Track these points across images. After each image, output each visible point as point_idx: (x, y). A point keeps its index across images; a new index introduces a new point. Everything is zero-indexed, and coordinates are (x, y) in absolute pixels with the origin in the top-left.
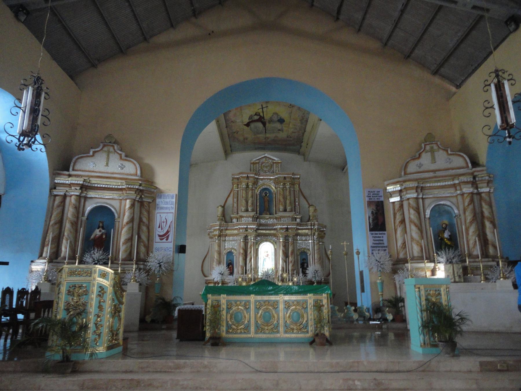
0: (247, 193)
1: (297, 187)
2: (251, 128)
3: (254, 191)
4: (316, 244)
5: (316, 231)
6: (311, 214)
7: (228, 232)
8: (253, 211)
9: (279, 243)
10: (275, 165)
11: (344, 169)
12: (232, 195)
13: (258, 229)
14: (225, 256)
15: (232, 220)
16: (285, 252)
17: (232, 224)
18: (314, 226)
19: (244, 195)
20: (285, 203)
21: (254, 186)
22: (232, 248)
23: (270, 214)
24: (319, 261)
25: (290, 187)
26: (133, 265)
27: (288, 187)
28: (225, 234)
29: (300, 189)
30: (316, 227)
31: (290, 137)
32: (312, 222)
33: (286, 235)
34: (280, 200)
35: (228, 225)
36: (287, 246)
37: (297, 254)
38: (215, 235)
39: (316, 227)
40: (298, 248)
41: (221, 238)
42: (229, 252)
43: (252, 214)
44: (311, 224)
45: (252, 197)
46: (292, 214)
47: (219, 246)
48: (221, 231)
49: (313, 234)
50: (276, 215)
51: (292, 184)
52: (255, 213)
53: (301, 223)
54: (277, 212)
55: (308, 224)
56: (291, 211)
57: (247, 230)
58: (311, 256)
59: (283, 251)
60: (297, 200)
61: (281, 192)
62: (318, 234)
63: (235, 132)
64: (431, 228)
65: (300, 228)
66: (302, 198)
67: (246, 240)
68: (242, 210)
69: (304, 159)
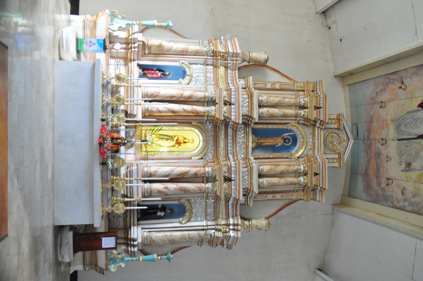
0: (289, 106)
1: (300, 195)
2: (416, 111)
3: (295, 118)
4: (199, 234)
5: (224, 234)
6: (254, 222)
7: (222, 70)
8: (260, 117)
9: (202, 165)
10: (336, 156)
11: (321, 271)
12: (285, 80)
13: (227, 125)
14: (177, 64)
15: (243, 78)
16: (186, 176)
17: (237, 78)
18: (234, 230)
19: (287, 100)
20: (274, 176)
21: (301, 119)
22: (191, 76)
23: (253, 149)
24: (168, 239)
25: (299, 184)
26: (136, 183)
27: (302, 179)
28: (219, 66)
29: (295, 201)
30: (232, 233)
31: (388, 184)
32: (241, 226)
33: (217, 178)
34: (278, 165)
35: (235, 70)
36: (196, 180)
37: (181, 198)
38: (216, 45)
39: (232, 233)
40: (193, 200)
41: (211, 56)
42: (185, 72)
43: (256, 116)
44: (237, 225)
45: (285, 116)
46: (256, 190)
47: (197, 53)
48: (223, 56)
49: (219, 227)
50: (252, 158)
51: (304, 187)
52: (257, 120)
53: (239, 204)
54: (257, 161)
55: (238, 221)
56: (259, 187)
57: (225, 104)
58: (178, 225)
59: (186, 173)
60: (278, 196)
61: (292, 167)
62: (218, 238)
63: (403, 83)
64: (145, 207)
65: (230, 204)
66: (281, 204)
67: (208, 102)
68: (261, 96)
69: (334, 205)
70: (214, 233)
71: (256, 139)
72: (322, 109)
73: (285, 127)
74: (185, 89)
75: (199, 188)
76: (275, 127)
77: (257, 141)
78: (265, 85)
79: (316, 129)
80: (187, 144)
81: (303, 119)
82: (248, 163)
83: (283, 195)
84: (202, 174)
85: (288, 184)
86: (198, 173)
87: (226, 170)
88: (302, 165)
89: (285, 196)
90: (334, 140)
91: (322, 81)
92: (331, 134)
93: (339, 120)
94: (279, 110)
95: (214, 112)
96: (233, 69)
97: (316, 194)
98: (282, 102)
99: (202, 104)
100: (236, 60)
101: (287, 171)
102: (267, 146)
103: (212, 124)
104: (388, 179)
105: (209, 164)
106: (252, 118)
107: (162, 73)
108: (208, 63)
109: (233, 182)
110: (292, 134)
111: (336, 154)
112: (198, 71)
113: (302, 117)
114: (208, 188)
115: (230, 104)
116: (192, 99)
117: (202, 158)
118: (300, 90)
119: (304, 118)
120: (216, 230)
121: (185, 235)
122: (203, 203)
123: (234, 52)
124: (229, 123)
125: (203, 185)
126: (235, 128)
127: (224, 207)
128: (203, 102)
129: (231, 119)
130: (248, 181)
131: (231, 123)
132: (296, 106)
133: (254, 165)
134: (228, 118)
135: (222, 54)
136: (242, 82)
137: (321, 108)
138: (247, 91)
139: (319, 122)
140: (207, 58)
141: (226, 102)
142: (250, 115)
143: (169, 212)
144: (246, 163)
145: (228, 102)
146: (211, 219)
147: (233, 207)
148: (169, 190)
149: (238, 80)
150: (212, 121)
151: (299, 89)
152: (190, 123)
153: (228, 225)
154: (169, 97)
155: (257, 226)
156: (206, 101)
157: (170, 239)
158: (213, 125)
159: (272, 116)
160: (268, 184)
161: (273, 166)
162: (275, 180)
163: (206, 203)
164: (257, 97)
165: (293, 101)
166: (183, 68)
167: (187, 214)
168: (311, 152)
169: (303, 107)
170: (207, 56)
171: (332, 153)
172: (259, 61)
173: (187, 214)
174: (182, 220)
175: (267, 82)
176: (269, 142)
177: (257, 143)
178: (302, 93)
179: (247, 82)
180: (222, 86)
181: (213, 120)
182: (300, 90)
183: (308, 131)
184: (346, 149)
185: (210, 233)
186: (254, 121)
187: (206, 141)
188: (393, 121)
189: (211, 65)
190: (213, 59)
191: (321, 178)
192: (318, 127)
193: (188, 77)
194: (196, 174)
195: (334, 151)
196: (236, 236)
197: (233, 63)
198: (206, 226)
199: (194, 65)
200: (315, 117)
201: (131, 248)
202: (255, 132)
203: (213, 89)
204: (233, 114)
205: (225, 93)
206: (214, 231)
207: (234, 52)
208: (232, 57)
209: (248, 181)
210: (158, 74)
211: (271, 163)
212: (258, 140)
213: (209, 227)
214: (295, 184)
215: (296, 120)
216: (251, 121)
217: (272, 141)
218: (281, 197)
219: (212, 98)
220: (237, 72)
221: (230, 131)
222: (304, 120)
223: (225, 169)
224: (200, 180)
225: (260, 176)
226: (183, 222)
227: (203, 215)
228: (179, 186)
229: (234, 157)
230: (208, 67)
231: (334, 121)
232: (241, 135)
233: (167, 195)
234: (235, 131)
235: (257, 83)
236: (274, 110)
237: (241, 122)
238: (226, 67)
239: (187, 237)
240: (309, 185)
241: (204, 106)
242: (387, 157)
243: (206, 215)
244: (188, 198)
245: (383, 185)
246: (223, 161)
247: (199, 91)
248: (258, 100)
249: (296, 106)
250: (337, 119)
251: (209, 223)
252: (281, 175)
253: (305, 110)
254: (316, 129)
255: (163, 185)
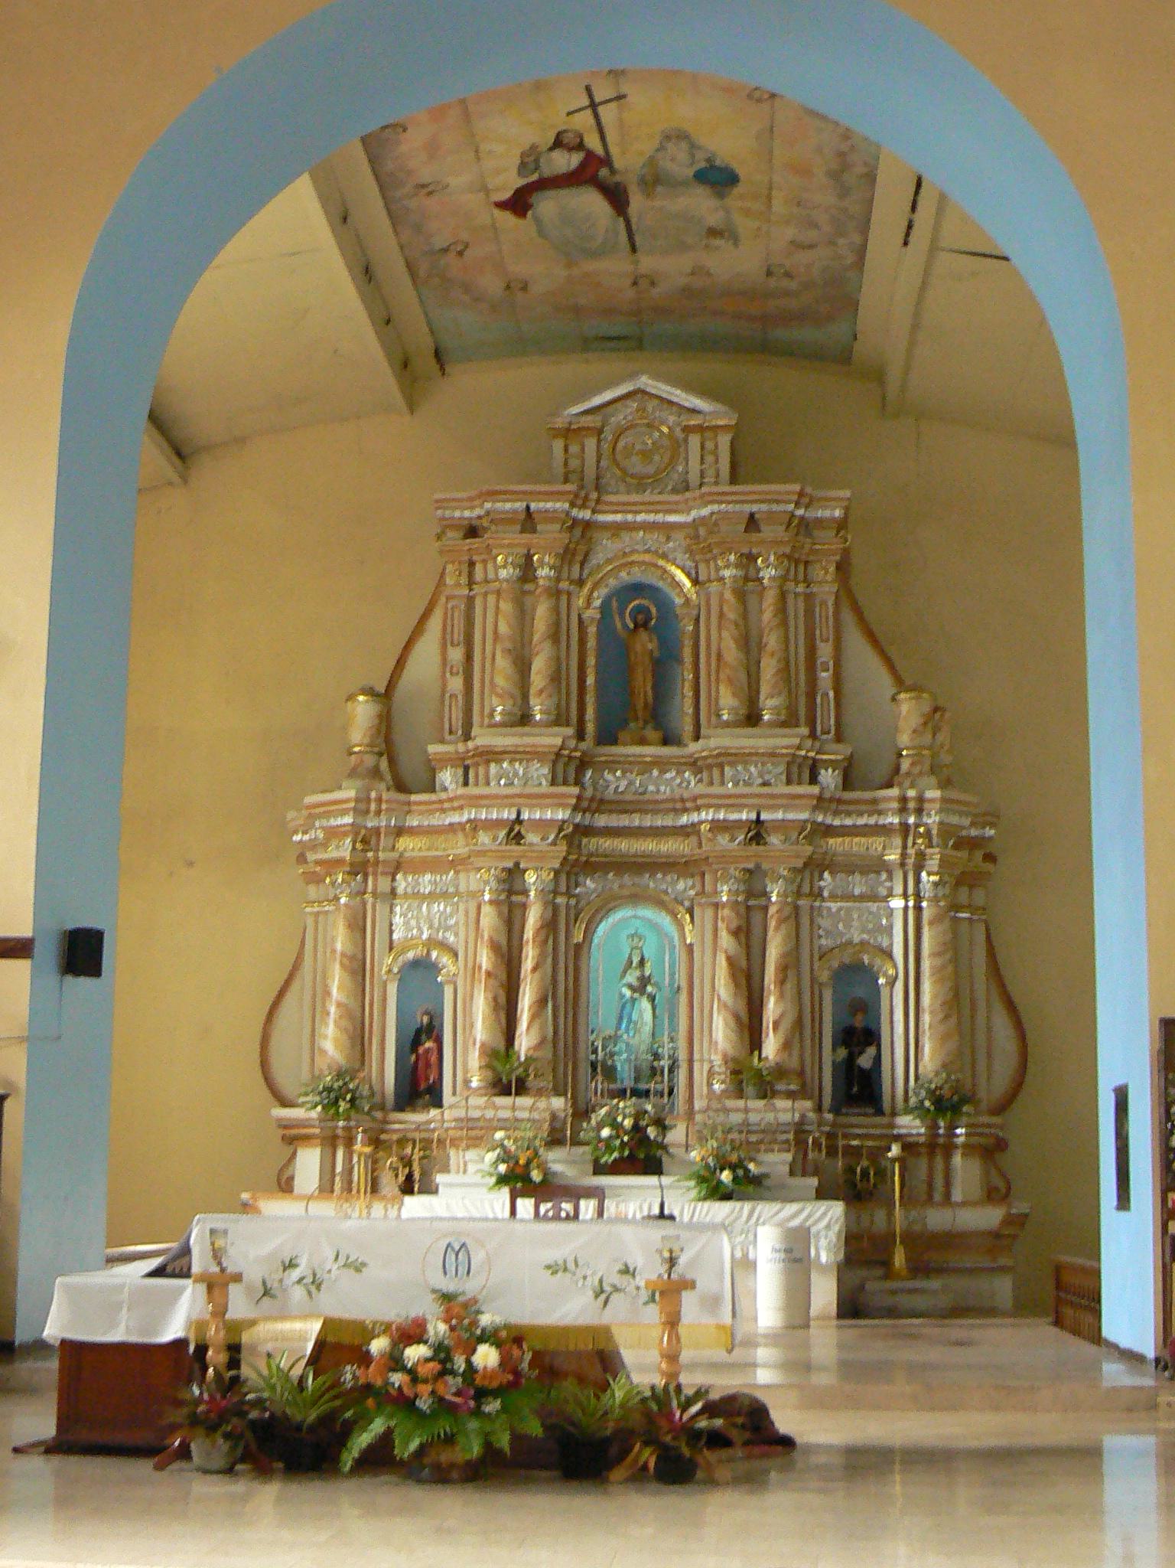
0: (523, 617)
3: (564, 598)
5: (935, 840)
10: (694, 440)
12: (435, 624)
14: (392, 989)
17: (433, 797)
21: (565, 575)
22: (431, 943)
23: (666, 741)
25: (785, 578)
27: (768, 574)
28: (395, 855)
30: (932, 819)
33: (751, 866)
34: (719, 656)
35: (409, 803)
36: (757, 930)
39: (932, 819)
40: (823, 941)
41: (365, 880)
42: (416, 964)
44: (904, 800)
47: (358, 925)
48: (364, 841)
49: (911, 861)
50: (693, 747)
51: (797, 562)
52: (570, 731)
55: (888, 799)
57: (519, 837)
58: (899, 986)
67: (511, 892)
70: (929, 874)
71: (632, 725)
72: (533, 506)
73: (592, 630)
74: (470, 964)
75: (780, 922)
76: (591, 661)
77: (641, 723)
78: (454, 700)
79: (601, 518)
80: (646, 956)
81: (566, 569)
82: (709, 761)
83: (821, 634)
84: (737, 914)
85: (784, 623)
86: (734, 925)
87: (727, 837)
88: (721, 573)
89: (825, 629)
90: (638, 447)
91: (437, 501)
92: (619, 457)
93: (568, 430)
94: (537, 654)
95: (544, 874)
96: (406, 808)
97: (819, 522)
98: (508, 645)
99: (517, 912)
100: (379, 800)
101: (736, 624)
102: (655, 687)
103: (581, 879)
104: (769, 273)
105: (708, 888)
106: (562, 748)
107: (424, 1037)
108: (388, 890)
109: (763, 817)
110: (615, 604)
111: (686, 440)
112: (413, 923)
113: (560, 572)
114: (783, 895)
115: (518, 820)
116: (504, 942)
117: (691, 911)
118: (471, 575)
119: (561, 566)
120: (919, 868)
121: (932, 967)
122: (834, 906)
123: (355, 809)
124: (577, 826)
125: (772, 910)
126: (594, 805)
127: (847, 840)
128: (511, 906)
129: (564, 822)
130: (763, 764)
131: (578, 819)
132: (524, 593)
133: (713, 743)
134: (561, 830)
135: (359, 846)
136: (447, 777)
137: (528, 508)
138: (477, 765)
139: (575, 512)
140: (374, 894)
141: (513, 834)
142: (553, 757)
143: (859, 1017)
144: (710, 767)
145: (511, 830)
146: (888, 884)
147: (849, 814)
148: (782, 1015)
149: (443, 796)
150: (573, 878)
151: (464, 580)
152: (578, 947)
153: (905, 828)
154: (497, 1015)
155: (914, 731)
156: (508, 897)
157: (941, 1016)
158: (586, 875)
159: (556, 678)
160: (780, 694)
161: (722, 676)
162: (769, 668)
163: (833, 897)
164: (493, 730)
165: (506, 606)
166: (403, 966)
167: (866, 962)
168: (679, 537)
169: (527, 570)
170: (365, 893)
171: (683, 455)
172: (377, 721)
173: (866, 959)
174: (885, 975)
175: (443, 696)
176: (643, 684)
177: (646, 722)
178: (479, 569)
179: (446, 761)
180: (459, 846)
181: (568, 874)
182: (471, 575)
183: (606, 548)
184: (671, 403)
185: (928, 886)
186: (572, 743)
187: (636, 898)
188: (569, 265)
189: (394, 880)
190: (375, 874)
191: (764, 507)
192: (594, 512)
193: (434, 954)
194: (735, 933)
195: (676, 447)
196: (937, 806)
197: (387, 810)
198: (907, 901)
199: (395, 936)
200: (557, 527)
201: (958, 1136)
202: (608, 737)
203: (472, 875)
204: (549, 815)
205: (484, 838)
206: (924, 874)
207: (355, 809)
208: (367, 812)
209: (763, 764)
210: (427, 1051)
211: (713, 678)
212: (636, 719)
213: (911, 890)
214: (783, 596)
215: (569, 594)
216: (573, 750)
217: (639, 671)
218: (827, 640)
219: (499, 881)
220: (414, 798)
221: (602, 820)
222: (570, 563)
223: (723, 840)
224: (757, 918)
225: (752, 719)
226: (891, 972)
227: (873, 906)
228: (772, 987)
229: (685, 810)
230: (400, 890)
231: (574, 449)
232: (616, 782)
233: (799, 1023)
234: (600, 805)
235: (447, 726)
236: (537, 674)
237: (575, 790)
238: (400, 831)
239: (938, 962)
240: (788, 550)
241: (524, 907)
242: (693, 274)
243: (874, 897)
244: (816, 957)
245: (793, 285)
246: (700, 845)
247: (478, 921)
248: (506, 726)
249: (524, 593)
250: (566, 438)
251: (899, 889)
252: (749, 644)
253: (536, 565)
254: (601, 518)
255: (767, 1035)
